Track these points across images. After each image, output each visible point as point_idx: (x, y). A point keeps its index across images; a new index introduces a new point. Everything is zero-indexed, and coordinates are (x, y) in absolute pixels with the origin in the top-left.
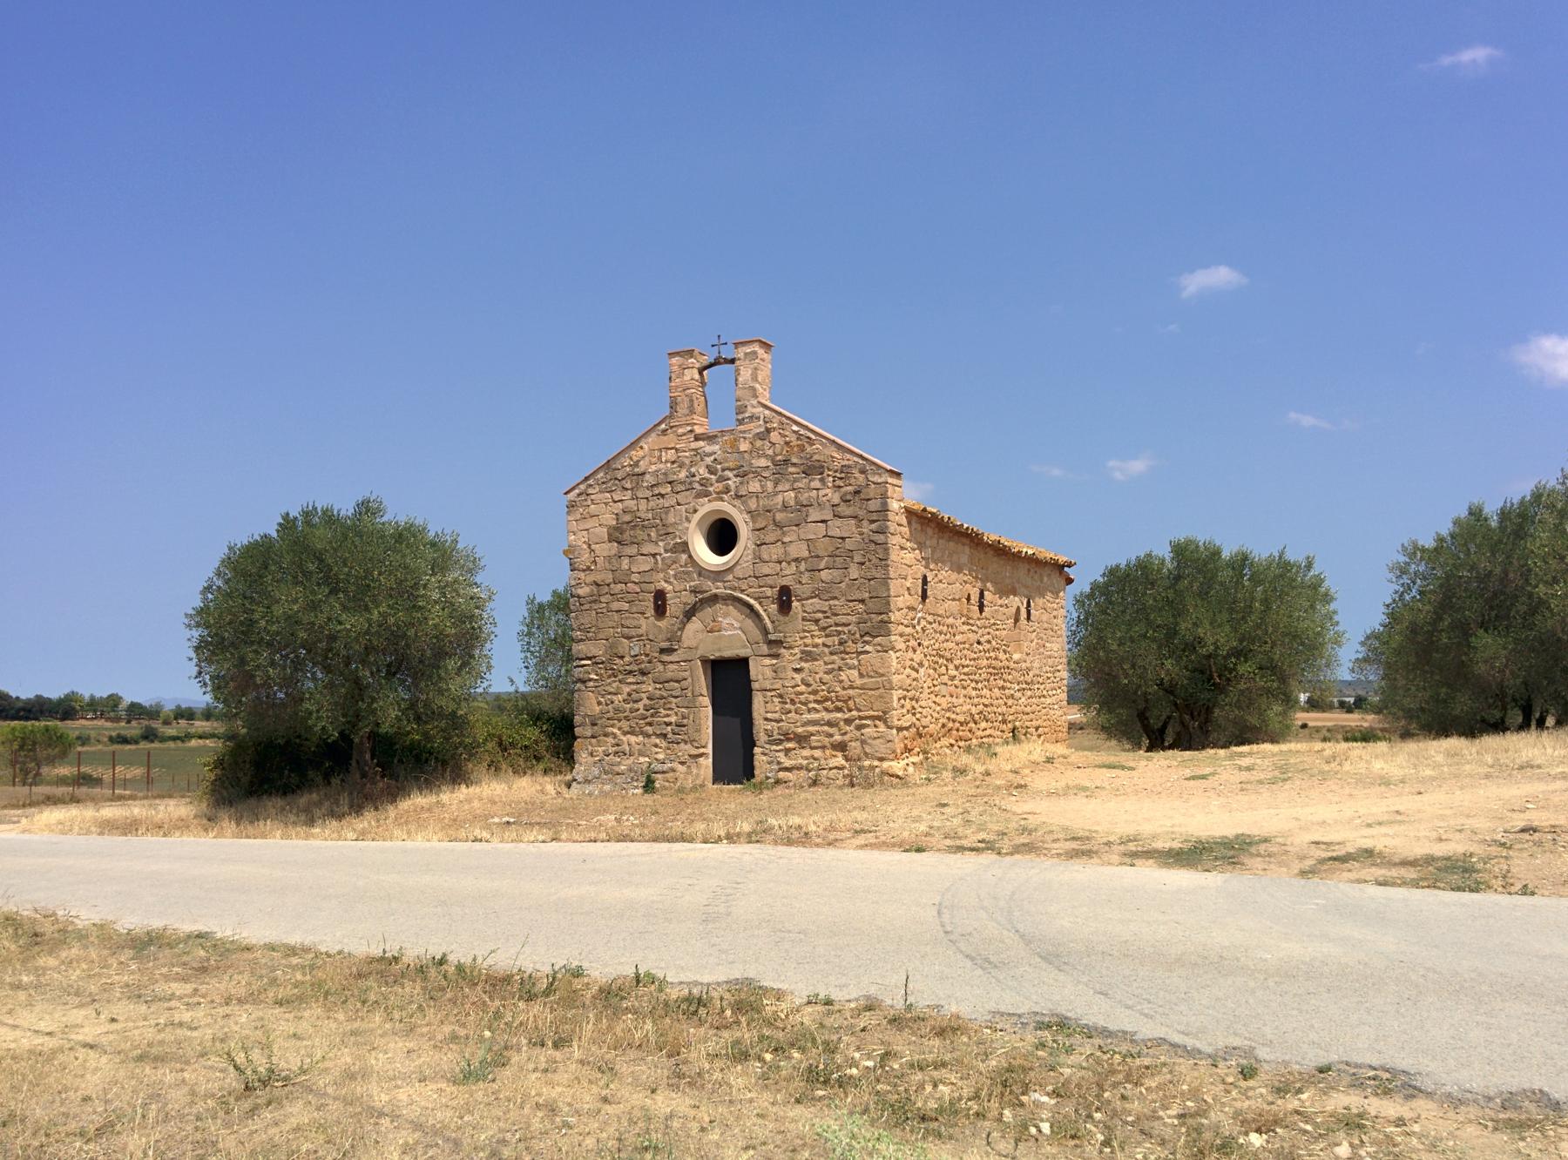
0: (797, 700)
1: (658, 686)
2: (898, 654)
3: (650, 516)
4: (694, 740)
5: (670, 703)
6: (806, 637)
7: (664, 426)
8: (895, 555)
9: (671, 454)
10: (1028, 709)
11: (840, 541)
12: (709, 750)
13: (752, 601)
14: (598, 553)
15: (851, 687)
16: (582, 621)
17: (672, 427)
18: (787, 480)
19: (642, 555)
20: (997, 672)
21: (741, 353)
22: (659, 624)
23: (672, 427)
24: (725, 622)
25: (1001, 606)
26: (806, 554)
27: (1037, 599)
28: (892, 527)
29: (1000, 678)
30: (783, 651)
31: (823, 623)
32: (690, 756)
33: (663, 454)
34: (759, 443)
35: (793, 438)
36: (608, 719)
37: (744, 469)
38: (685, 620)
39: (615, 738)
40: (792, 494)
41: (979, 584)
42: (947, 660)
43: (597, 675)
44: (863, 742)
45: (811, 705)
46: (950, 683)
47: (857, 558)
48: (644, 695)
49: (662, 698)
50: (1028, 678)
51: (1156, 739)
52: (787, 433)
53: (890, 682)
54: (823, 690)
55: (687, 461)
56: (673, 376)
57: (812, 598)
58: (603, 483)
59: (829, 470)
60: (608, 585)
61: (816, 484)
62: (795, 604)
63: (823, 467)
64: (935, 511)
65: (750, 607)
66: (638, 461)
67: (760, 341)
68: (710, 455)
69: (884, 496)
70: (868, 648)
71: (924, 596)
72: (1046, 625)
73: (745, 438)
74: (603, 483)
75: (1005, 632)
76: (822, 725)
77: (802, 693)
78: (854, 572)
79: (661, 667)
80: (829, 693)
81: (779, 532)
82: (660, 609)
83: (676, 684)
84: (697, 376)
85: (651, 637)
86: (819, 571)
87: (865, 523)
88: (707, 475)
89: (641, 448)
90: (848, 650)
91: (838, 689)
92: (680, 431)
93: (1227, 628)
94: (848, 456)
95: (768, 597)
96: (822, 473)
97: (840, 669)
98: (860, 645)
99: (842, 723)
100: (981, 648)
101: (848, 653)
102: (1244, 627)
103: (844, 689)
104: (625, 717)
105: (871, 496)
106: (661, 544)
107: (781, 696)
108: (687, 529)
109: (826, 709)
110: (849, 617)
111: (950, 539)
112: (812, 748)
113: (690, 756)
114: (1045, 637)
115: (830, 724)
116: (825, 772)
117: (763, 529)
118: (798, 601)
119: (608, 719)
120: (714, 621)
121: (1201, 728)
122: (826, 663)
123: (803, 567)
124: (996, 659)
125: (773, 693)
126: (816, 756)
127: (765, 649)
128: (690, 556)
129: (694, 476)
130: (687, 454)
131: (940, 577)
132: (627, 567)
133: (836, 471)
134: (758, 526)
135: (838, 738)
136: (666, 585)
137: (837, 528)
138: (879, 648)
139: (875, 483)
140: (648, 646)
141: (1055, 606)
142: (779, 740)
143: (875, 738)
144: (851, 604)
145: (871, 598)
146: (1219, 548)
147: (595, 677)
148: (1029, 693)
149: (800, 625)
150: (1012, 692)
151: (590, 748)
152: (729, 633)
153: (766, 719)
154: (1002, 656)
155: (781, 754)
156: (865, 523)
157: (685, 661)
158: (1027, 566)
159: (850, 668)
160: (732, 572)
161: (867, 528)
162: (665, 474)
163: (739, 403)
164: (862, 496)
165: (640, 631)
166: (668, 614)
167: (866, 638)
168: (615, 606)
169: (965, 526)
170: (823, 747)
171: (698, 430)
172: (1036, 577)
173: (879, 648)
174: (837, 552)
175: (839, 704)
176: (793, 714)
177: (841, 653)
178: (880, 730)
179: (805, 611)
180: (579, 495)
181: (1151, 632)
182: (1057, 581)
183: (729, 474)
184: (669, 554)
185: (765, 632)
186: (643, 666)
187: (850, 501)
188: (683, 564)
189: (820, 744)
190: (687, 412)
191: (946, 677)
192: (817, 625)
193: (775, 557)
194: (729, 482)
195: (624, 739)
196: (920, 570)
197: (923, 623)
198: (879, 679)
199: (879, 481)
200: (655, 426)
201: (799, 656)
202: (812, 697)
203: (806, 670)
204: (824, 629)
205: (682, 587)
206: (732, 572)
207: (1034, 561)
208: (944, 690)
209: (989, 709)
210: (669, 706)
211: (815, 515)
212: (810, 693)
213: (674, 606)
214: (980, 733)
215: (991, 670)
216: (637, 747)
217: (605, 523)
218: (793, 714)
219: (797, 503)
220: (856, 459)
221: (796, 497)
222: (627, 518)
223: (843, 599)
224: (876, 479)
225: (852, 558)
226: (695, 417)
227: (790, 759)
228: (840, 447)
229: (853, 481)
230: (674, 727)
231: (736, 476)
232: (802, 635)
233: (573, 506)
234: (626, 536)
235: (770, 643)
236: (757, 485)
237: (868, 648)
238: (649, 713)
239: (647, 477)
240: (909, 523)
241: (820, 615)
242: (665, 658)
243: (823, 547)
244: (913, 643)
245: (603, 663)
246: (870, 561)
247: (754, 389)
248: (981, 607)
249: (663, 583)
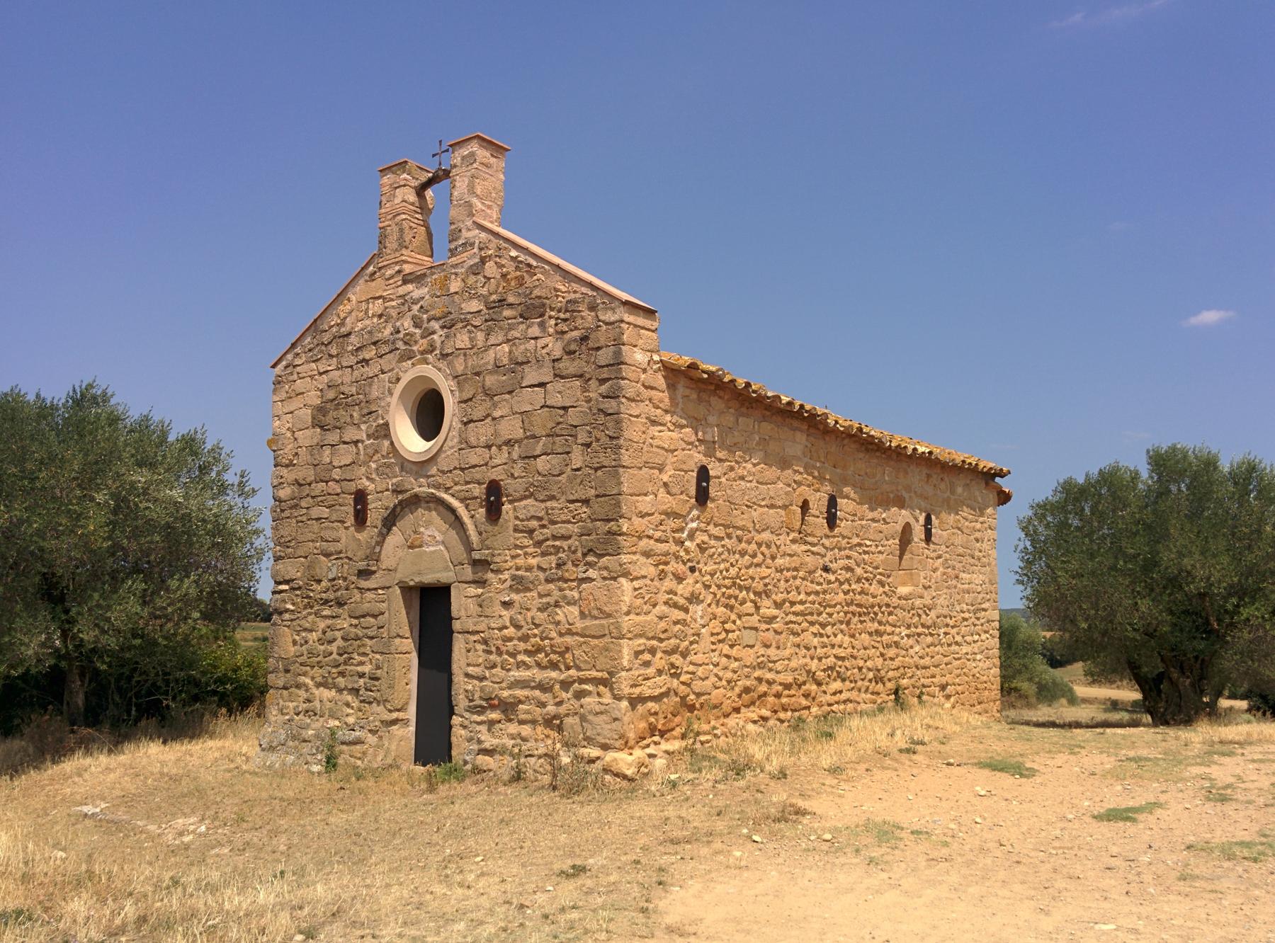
0: (504, 649)
1: (355, 622)
2: (636, 584)
3: (354, 390)
4: (386, 700)
5: (364, 645)
6: (519, 555)
7: (369, 270)
8: (633, 431)
9: (377, 307)
10: (927, 661)
11: (562, 412)
12: (411, 713)
13: (455, 503)
14: (301, 442)
15: (570, 633)
16: (282, 532)
17: (380, 269)
18: (501, 328)
19: (345, 443)
20: (866, 612)
21: (457, 157)
22: (359, 536)
23: (380, 269)
24: (427, 532)
25: (873, 520)
26: (519, 433)
27: (943, 515)
28: (630, 389)
29: (873, 620)
30: (490, 575)
31: (538, 535)
32: (382, 722)
33: (371, 306)
34: (471, 279)
35: (510, 267)
36: (301, 664)
37: (452, 317)
38: (385, 531)
39: (307, 691)
40: (506, 348)
41: (828, 488)
42: (756, 593)
43: (293, 604)
44: (583, 719)
45: (520, 657)
46: (764, 626)
47: (582, 437)
48: (338, 634)
49: (357, 638)
50: (928, 620)
51: (1151, 689)
52: (504, 262)
53: (618, 628)
54: (535, 636)
55: (394, 313)
56: (384, 199)
57: (525, 497)
58: (310, 350)
59: (552, 309)
60: (310, 484)
61: (535, 331)
62: (507, 507)
63: (544, 305)
64: (713, 368)
65: (452, 510)
66: (345, 318)
67: (478, 137)
68: (415, 302)
69: (618, 343)
70: (592, 573)
71: (702, 497)
72: (961, 550)
73: (456, 274)
74: (310, 350)
75: (882, 557)
76: (533, 688)
77: (510, 639)
78: (577, 459)
79: (357, 596)
80: (542, 640)
81: (489, 404)
82: (361, 518)
83: (372, 620)
84: (412, 197)
85: (349, 554)
86: (535, 457)
87: (593, 383)
88: (412, 330)
89: (349, 300)
90: (567, 575)
91: (553, 634)
92: (389, 272)
93: (1225, 560)
94: (575, 286)
95: (476, 498)
96: (542, 315)
97: (557, 605)
98: (582, 568)
99: (557, 687)
100: (832, 578)
101: (566, 581)
102: (1250, 558)
103: (561, 635)
104: (319, 662)
105: (602, 342)
106: (363, 427)
107: (485, 642)
108: (389, 404)
109: (538, 665)
110: (569, 526)
111: (764, 419)
112: (521, 722)
113: (382, 722)
114: (958, 565)
115: (544, 687)
116: (532, 760)
117: (470, 399)
118: (511, 502)
119: (301, 664)
120: (415, 532)
121: (1192, 685)
122: (540, 596)
123: (516, 453)
124: (862, 592)
125: (476, 637)
126: (524, 734)
127: (468, 572)
128: (392, 443)
129: (398, 332)
130: (394, 303)
131: (740, 472)
132: (328, 460)
133: (559, 311)
134: (466, 395)
135: (551, 709)
136: (367, 483)
137: (560, 393)
138: (605, 573)
139: (607, 324)
140: (346, 567)
141: (978, 526)
142: (481, 706)
143: (597, 713)
144: (572, 506)
145: (597, 496)
146: (1216, 456)
147: (291, 607)
148: (929, 639)
149: (511, 537)
150: (896, 638)
151: (281, 702)
152: (432, 549)
153: (467, 675)
154: (874, 588)
155: (483, 728)
156: (593, 383)
157: (383, 588)
158: (925, 471)
159: (569, 604)
160: (436, 464)
161: (596, 390)
162: (370, 332)
163: (453, 227)
164: (591, 345)
165: (339, 546)
166: (368, 523)
167: (590, 558)
168: (315, 512)
169: (785, 399)
170: (533, 722)
171: (408, 268)
172: (943, 486)
173: (605, 573)
174: (557, 430)
175: (554, 657)
176: (499, 669)
177: (559, 579)
178: (605, 700)
179: (517, 518)
180: (286, 367)
181: (1121, 563)
182: (980, 492)
183: (435, 325)
184: (372, 441)
185: (469, 548)
186: (339, 593)
187: (575, 352)
188: (385, 453)
189: (529, 717)
190: (395, 245)
191: (756, 618)
192: (532, 538)
193: (483, 439)
194: (435, 337)
195: (316, 692)
196: (697, 457)
197: (701, 537)
198: (604, 622)
199: (613, 319)
200: (363, 269)
201: (508, 583)
202: (522, 646)
203: (517, 605)
204: (538, 544)
205: (384, 486)
206: (436, 464)
207: (929, 462)
208: (749, 637)
209: (847, 663)
210: (362, 650)
211: (532, 376)
212: (520, 639)
213: (376, 510)
214: (828, 698)
215: (853, 608)
216: (328, 705)
217: (310, 402)
218: (499, 669)
219: (511, 360)
220: (584, 290)
221: (510, 352)
222: (331, 394)
223: (563, 499)
224: (609, 316)
225: (575, 436)
226: (404, 251)
227: (494, 737)
228: (566, 274)
229: (579, 321)
230: (367, 680)
231: (443, 327)
232: (514, 552)
233: (279, 383)
234: (329, 419)
235: (475, 563)
236: (466, 337)
237: (592, 573)
238: (341, 659)
239: (353, 338)
240: (671, 387)
241: (534, 523)
242: (364, 584)
243: (541, 423)
244: (674, 566)
245: (299, 588)
246: (598, 440)
247: (469, 205)
248: (832, 521)
249: (364, 480)
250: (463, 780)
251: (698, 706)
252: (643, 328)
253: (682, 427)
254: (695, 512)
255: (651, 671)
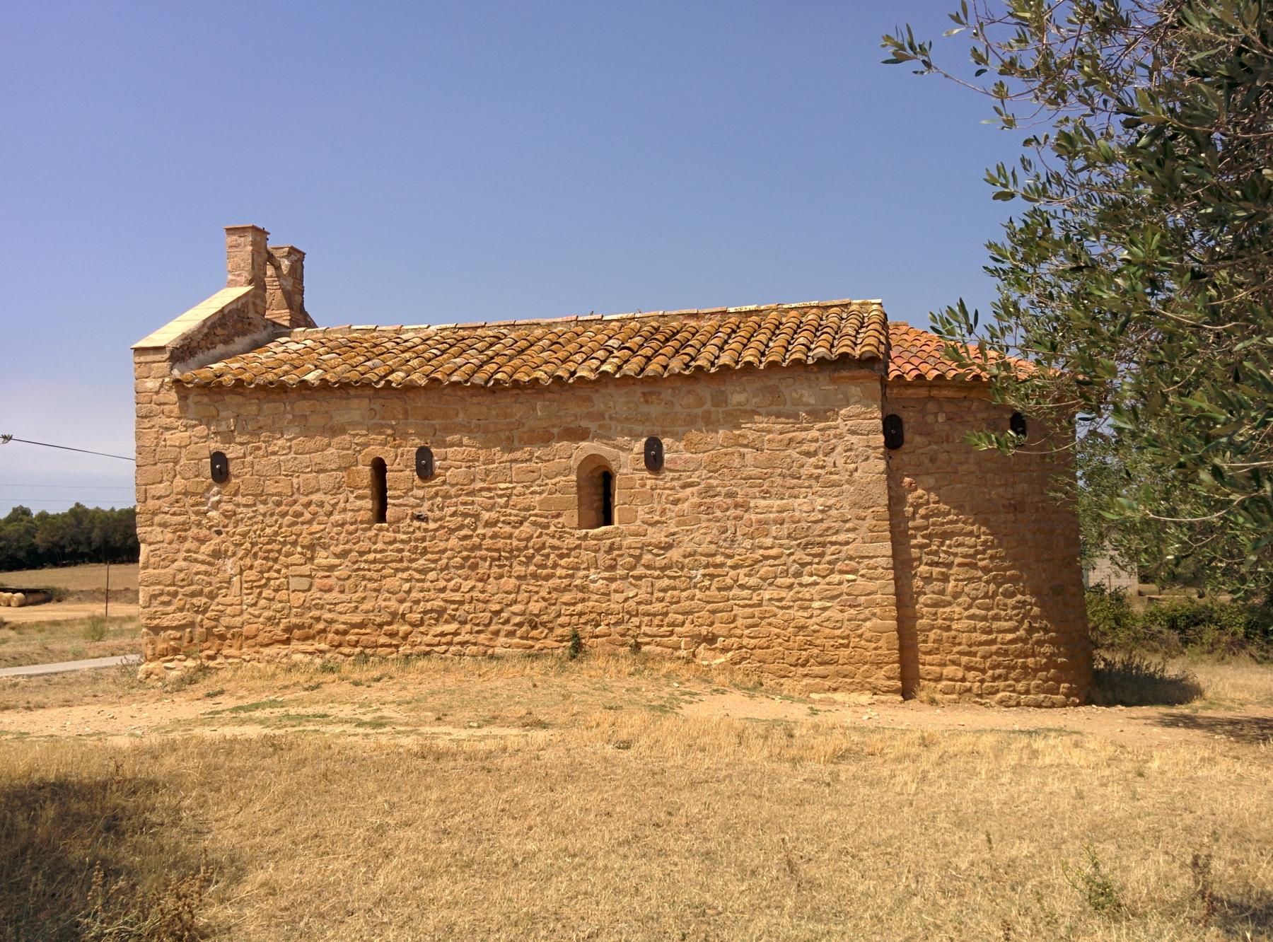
250: (1098, 585)
251: (229, 636)
252: (154, 362)
253: (195, 426)
254: (215, 489)
255: (170, 609)
